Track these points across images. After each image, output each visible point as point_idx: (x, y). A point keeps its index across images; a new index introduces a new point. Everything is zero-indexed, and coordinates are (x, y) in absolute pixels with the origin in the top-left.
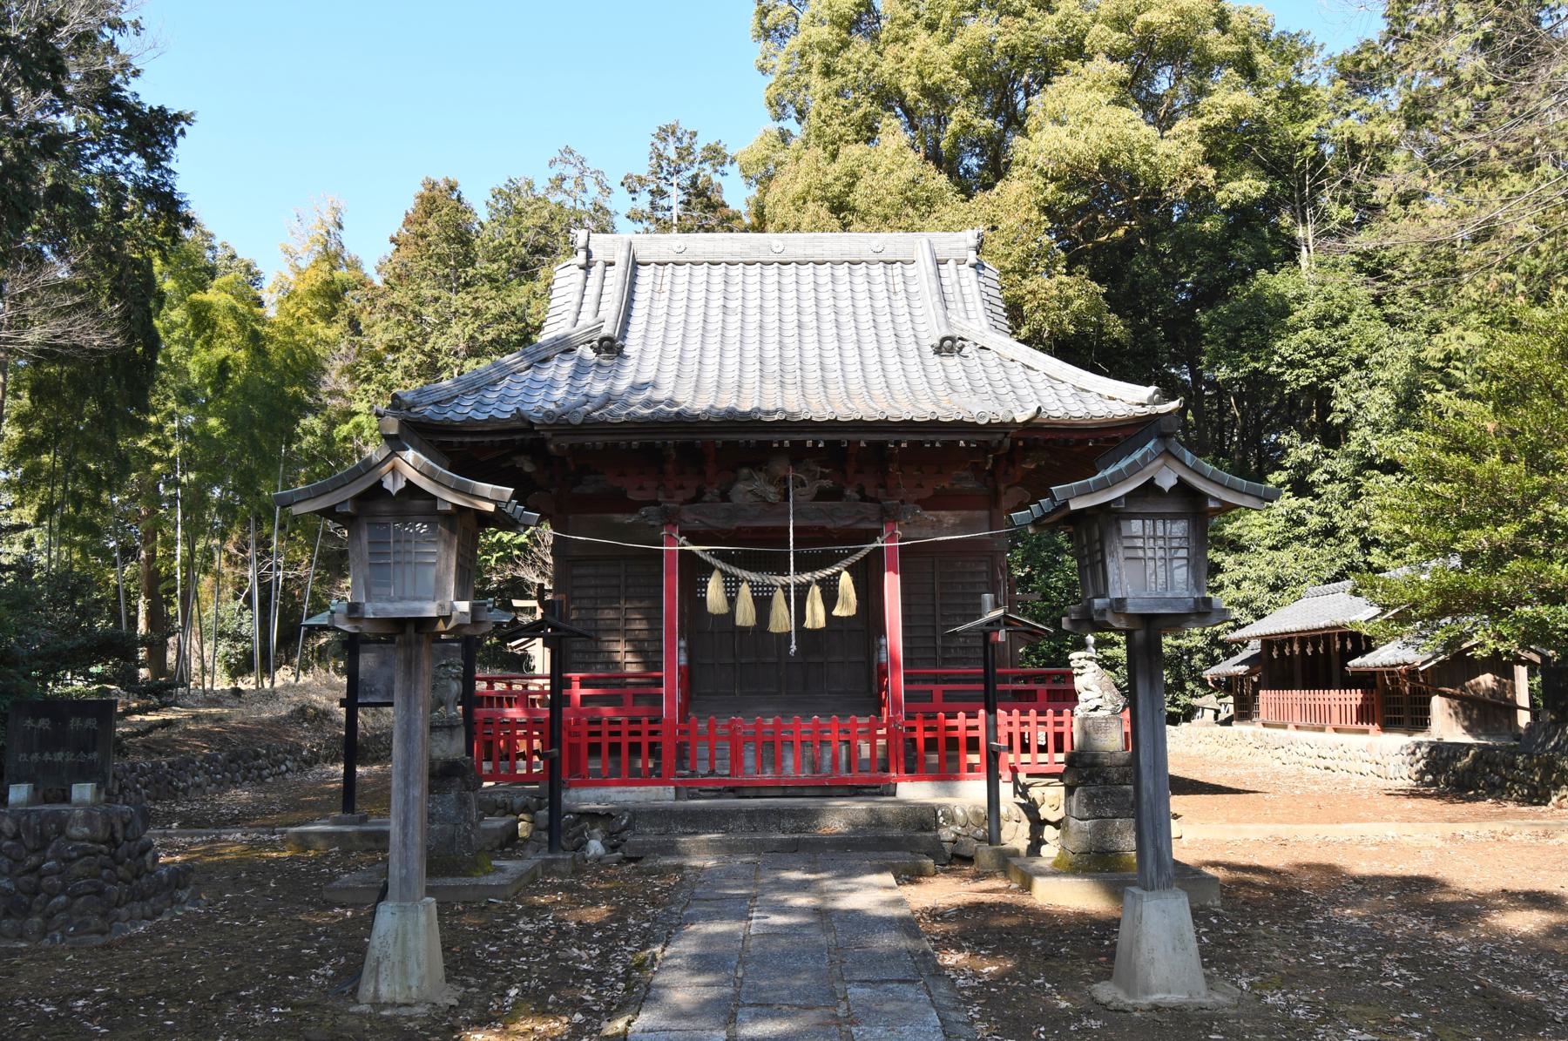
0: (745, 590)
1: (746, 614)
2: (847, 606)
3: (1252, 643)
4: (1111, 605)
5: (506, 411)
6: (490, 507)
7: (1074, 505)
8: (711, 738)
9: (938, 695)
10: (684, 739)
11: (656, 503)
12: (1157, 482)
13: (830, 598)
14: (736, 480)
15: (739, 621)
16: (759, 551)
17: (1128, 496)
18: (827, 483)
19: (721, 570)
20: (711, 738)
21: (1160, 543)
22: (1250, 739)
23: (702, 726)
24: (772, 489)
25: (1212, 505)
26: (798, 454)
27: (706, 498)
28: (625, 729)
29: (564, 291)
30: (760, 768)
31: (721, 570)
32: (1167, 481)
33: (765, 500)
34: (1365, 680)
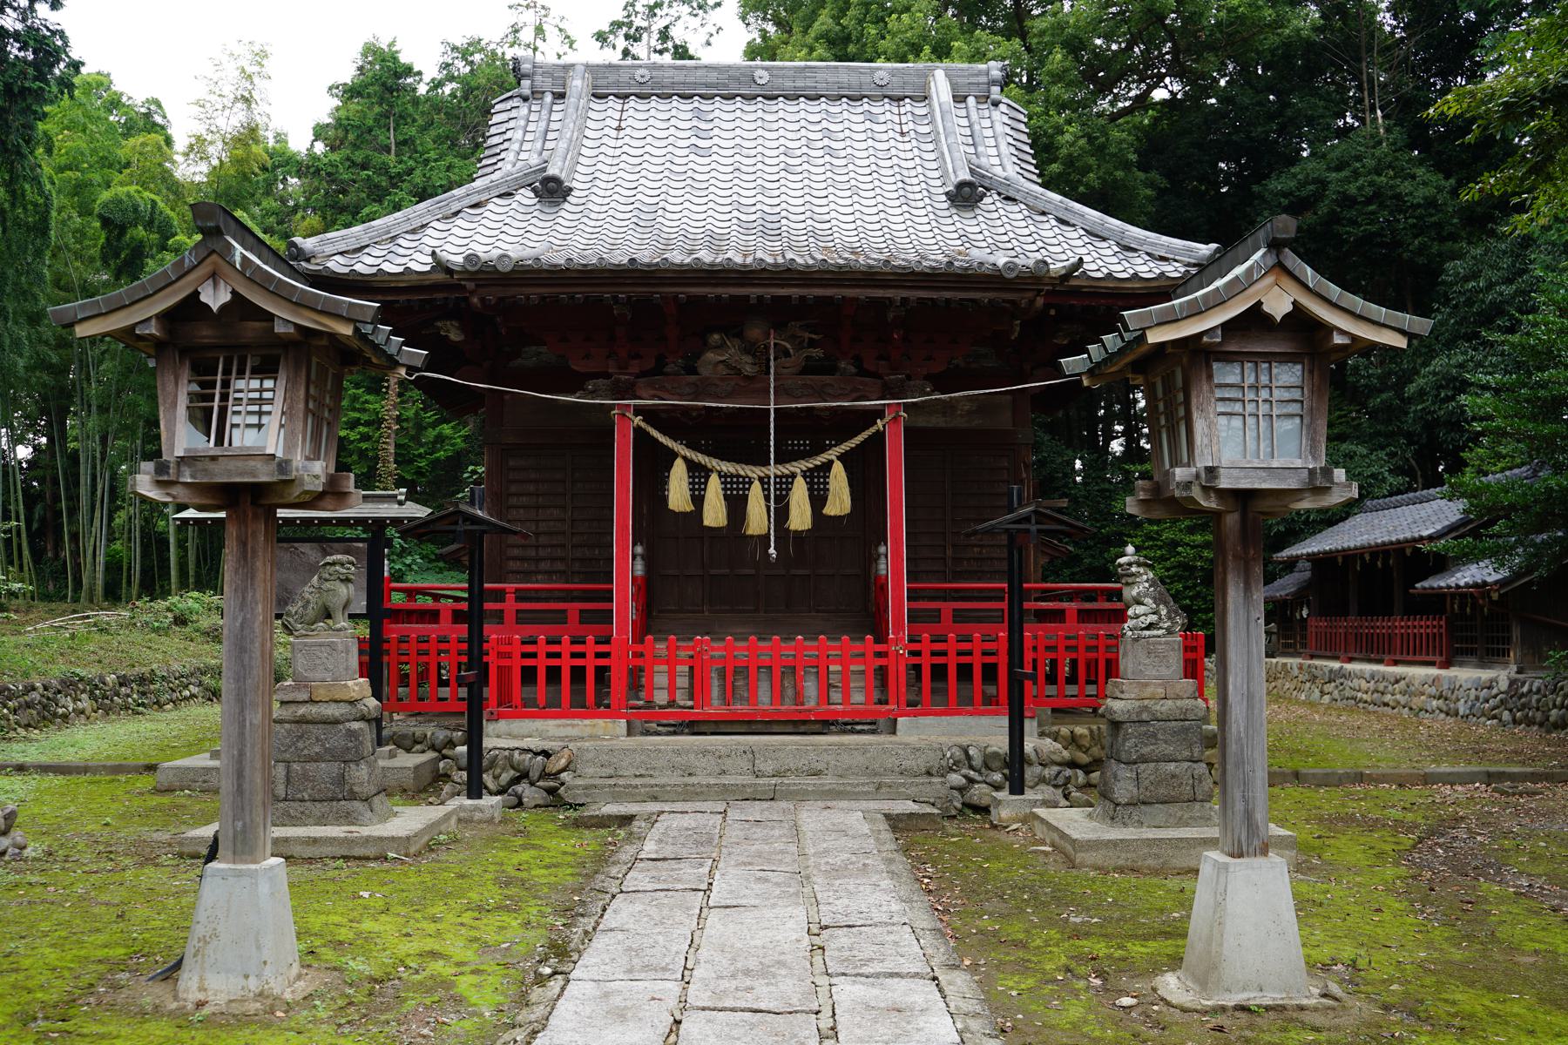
0: (714, 484)
1: (715, 513)
2: (840, 501)
3: (1300, 564)
4: (1197, 476)
5: (421, 263)
6: (346, 330)
7: (1155, 337)
8: (671, 662)
9: (947, 615)
10: (639, 662)
11: (607, 376)
12: (1265, 308)
14: (706, 346)
15: (709, 520)
17: (1226, 326)
18: (817, 353)
19: (685, 458)
20: (671, 662)
21: (1264, 394)
22: (1296, 672)
23: (661, 647)
25: (1338, 340)
27: (667, 369)
30: (726, 699)
31: (685, 458)
32: (215, 298)
33: (739, 372)
34: (1437, 603)
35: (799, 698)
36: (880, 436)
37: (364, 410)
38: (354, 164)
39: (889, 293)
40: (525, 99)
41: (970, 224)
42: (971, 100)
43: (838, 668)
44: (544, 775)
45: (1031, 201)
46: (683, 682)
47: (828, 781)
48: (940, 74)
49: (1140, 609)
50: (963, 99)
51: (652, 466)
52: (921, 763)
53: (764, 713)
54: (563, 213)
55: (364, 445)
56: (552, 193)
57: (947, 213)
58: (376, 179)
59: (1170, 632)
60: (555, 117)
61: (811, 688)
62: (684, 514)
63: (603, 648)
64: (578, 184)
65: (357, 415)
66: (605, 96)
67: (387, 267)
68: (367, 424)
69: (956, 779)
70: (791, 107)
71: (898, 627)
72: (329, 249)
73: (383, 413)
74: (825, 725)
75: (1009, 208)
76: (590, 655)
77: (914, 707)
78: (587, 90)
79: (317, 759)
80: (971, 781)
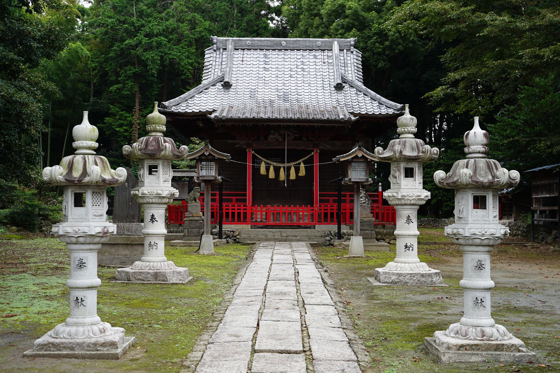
1: (272, 175)
2: (302, 173)
7: (341, 160)
8: (261, 211)
13: (297, 170)
16: (275, 155)
18: (297, 135)
20: (261, 211)
23: (259, 209)
24: (280, 137)
26: (288, 128)
28: (231, 208)
29: (209, 59)
30: (274, 220)
32: (207, 154)
35: (292, 220)
36: (313, 156)
37: (125, 120)
38: (120, 22)
39: (314, 124)
40: (215, 51)
41: (341, 96)
42: (345, 51)
43: (303, 213)
44: (233, 236)
45: (357, 88)
46: (264, 217)
47: (298, 238)
48: (336, 43)
49: (362, 199)
50: (343, 50)
51: (255, 160)
52: (320, 234)
53: (284, 223)
54: (230, 92)
55: (126, 134)
56: (227, 86)
57: (334, 92)
58: (130, 28)
59: (368, 204)
60: (224, 56)
61: (295, 218)
62: (264, 175)
63: (245, 208)
64: (233, 82)
65: (122, 122)
66: (238, 49)
67: (187, 110)
68: (126, 125)
69: (328, 238)
70: (292, 53)
71: (317, 203)
72: (171, 105)
73: (133, 121)
74: (299, 227)
75: (351, 90)
76: (236, 210)
77: (320, 223)
78: (233, 48)
79: (194, 228)
80: (331, 239)
